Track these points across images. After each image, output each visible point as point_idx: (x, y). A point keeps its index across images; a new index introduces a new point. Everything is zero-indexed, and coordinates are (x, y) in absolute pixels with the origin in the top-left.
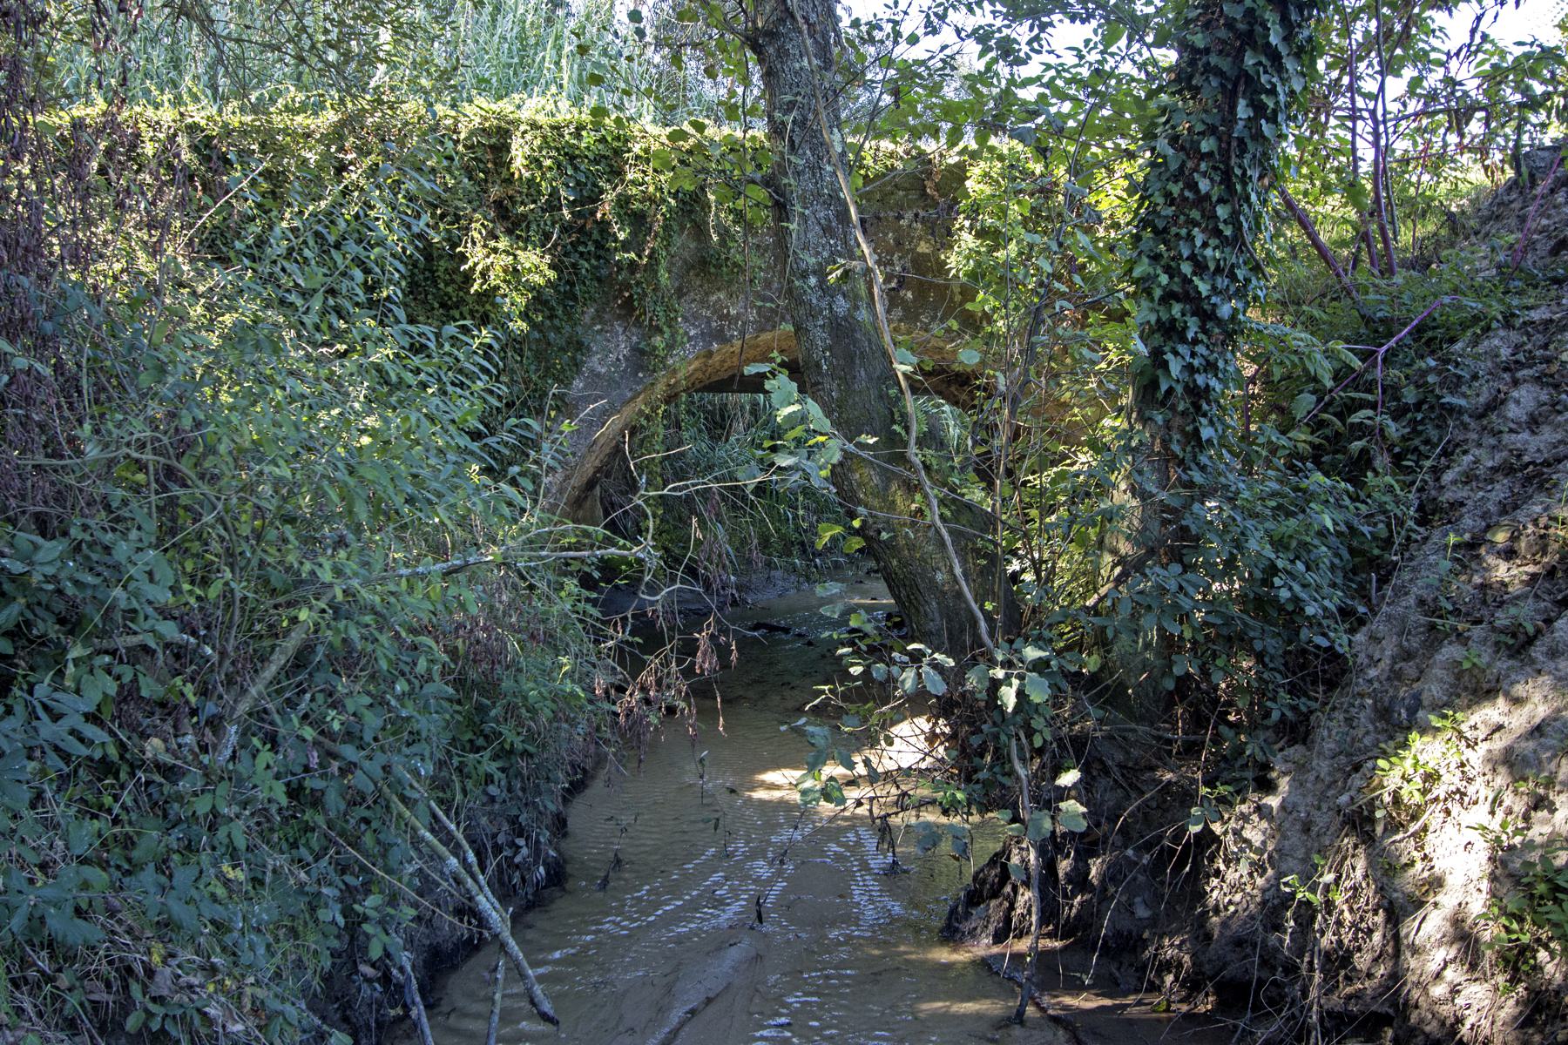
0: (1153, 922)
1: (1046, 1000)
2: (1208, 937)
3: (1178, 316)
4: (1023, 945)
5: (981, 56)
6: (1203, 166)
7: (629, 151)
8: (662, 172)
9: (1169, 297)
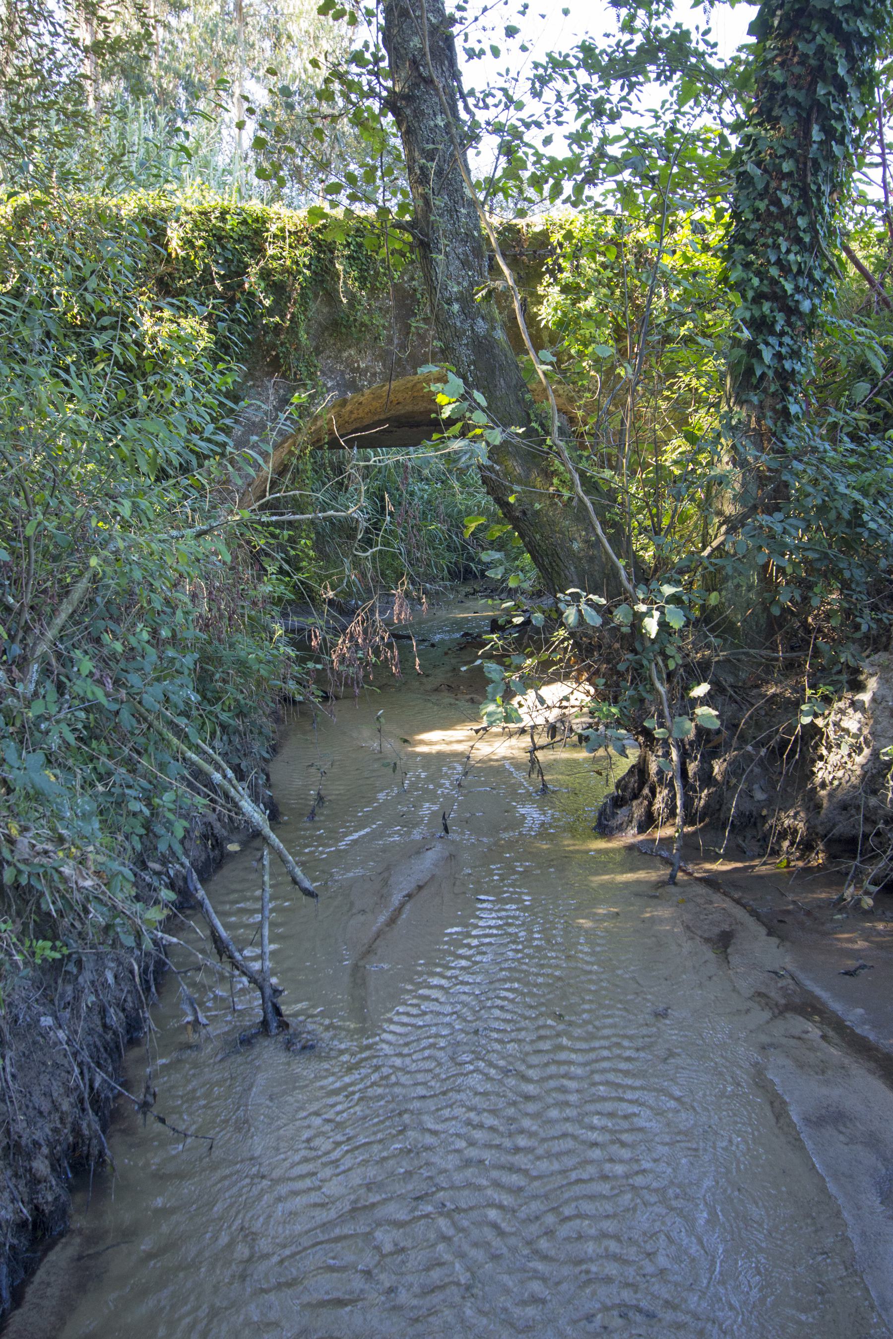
0: (770, 802)
1: (690, 867)
2: (819, 807)
3: (768, 312)
4: (667, 831)
5: (578, 117)
6: (784, 185)
7: (267, 231)
8: (296, 248)
9: (759, 297)
